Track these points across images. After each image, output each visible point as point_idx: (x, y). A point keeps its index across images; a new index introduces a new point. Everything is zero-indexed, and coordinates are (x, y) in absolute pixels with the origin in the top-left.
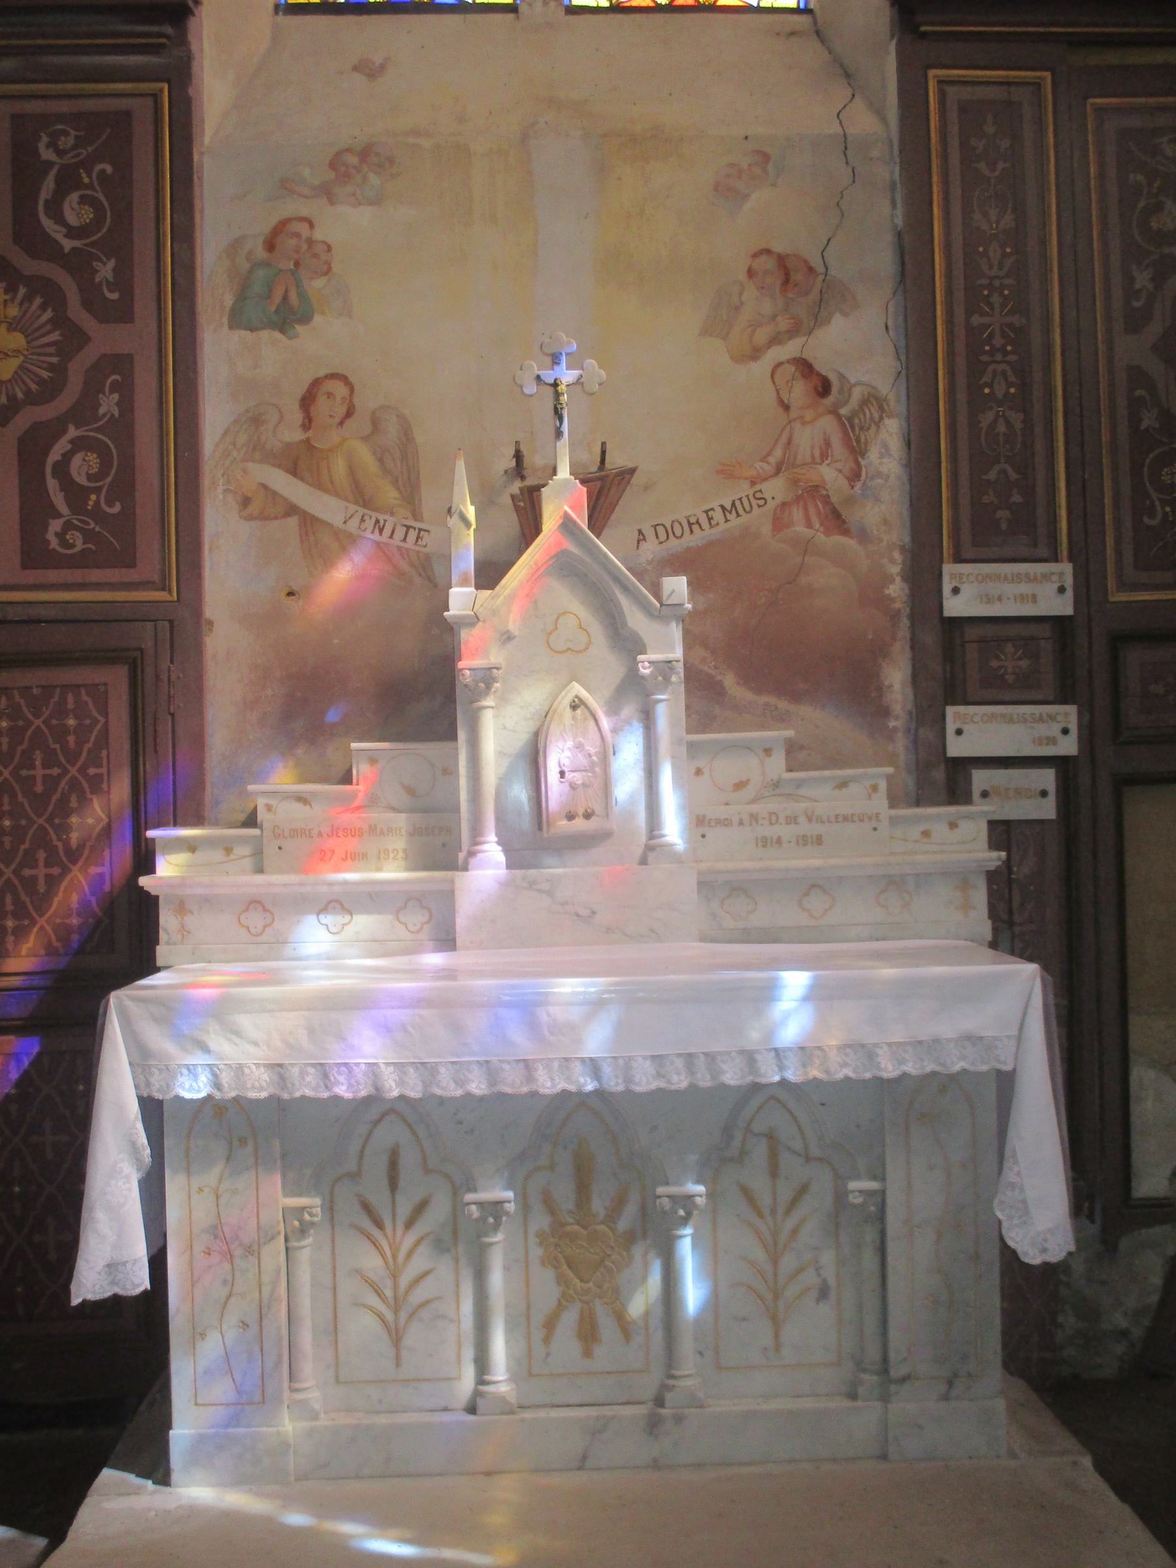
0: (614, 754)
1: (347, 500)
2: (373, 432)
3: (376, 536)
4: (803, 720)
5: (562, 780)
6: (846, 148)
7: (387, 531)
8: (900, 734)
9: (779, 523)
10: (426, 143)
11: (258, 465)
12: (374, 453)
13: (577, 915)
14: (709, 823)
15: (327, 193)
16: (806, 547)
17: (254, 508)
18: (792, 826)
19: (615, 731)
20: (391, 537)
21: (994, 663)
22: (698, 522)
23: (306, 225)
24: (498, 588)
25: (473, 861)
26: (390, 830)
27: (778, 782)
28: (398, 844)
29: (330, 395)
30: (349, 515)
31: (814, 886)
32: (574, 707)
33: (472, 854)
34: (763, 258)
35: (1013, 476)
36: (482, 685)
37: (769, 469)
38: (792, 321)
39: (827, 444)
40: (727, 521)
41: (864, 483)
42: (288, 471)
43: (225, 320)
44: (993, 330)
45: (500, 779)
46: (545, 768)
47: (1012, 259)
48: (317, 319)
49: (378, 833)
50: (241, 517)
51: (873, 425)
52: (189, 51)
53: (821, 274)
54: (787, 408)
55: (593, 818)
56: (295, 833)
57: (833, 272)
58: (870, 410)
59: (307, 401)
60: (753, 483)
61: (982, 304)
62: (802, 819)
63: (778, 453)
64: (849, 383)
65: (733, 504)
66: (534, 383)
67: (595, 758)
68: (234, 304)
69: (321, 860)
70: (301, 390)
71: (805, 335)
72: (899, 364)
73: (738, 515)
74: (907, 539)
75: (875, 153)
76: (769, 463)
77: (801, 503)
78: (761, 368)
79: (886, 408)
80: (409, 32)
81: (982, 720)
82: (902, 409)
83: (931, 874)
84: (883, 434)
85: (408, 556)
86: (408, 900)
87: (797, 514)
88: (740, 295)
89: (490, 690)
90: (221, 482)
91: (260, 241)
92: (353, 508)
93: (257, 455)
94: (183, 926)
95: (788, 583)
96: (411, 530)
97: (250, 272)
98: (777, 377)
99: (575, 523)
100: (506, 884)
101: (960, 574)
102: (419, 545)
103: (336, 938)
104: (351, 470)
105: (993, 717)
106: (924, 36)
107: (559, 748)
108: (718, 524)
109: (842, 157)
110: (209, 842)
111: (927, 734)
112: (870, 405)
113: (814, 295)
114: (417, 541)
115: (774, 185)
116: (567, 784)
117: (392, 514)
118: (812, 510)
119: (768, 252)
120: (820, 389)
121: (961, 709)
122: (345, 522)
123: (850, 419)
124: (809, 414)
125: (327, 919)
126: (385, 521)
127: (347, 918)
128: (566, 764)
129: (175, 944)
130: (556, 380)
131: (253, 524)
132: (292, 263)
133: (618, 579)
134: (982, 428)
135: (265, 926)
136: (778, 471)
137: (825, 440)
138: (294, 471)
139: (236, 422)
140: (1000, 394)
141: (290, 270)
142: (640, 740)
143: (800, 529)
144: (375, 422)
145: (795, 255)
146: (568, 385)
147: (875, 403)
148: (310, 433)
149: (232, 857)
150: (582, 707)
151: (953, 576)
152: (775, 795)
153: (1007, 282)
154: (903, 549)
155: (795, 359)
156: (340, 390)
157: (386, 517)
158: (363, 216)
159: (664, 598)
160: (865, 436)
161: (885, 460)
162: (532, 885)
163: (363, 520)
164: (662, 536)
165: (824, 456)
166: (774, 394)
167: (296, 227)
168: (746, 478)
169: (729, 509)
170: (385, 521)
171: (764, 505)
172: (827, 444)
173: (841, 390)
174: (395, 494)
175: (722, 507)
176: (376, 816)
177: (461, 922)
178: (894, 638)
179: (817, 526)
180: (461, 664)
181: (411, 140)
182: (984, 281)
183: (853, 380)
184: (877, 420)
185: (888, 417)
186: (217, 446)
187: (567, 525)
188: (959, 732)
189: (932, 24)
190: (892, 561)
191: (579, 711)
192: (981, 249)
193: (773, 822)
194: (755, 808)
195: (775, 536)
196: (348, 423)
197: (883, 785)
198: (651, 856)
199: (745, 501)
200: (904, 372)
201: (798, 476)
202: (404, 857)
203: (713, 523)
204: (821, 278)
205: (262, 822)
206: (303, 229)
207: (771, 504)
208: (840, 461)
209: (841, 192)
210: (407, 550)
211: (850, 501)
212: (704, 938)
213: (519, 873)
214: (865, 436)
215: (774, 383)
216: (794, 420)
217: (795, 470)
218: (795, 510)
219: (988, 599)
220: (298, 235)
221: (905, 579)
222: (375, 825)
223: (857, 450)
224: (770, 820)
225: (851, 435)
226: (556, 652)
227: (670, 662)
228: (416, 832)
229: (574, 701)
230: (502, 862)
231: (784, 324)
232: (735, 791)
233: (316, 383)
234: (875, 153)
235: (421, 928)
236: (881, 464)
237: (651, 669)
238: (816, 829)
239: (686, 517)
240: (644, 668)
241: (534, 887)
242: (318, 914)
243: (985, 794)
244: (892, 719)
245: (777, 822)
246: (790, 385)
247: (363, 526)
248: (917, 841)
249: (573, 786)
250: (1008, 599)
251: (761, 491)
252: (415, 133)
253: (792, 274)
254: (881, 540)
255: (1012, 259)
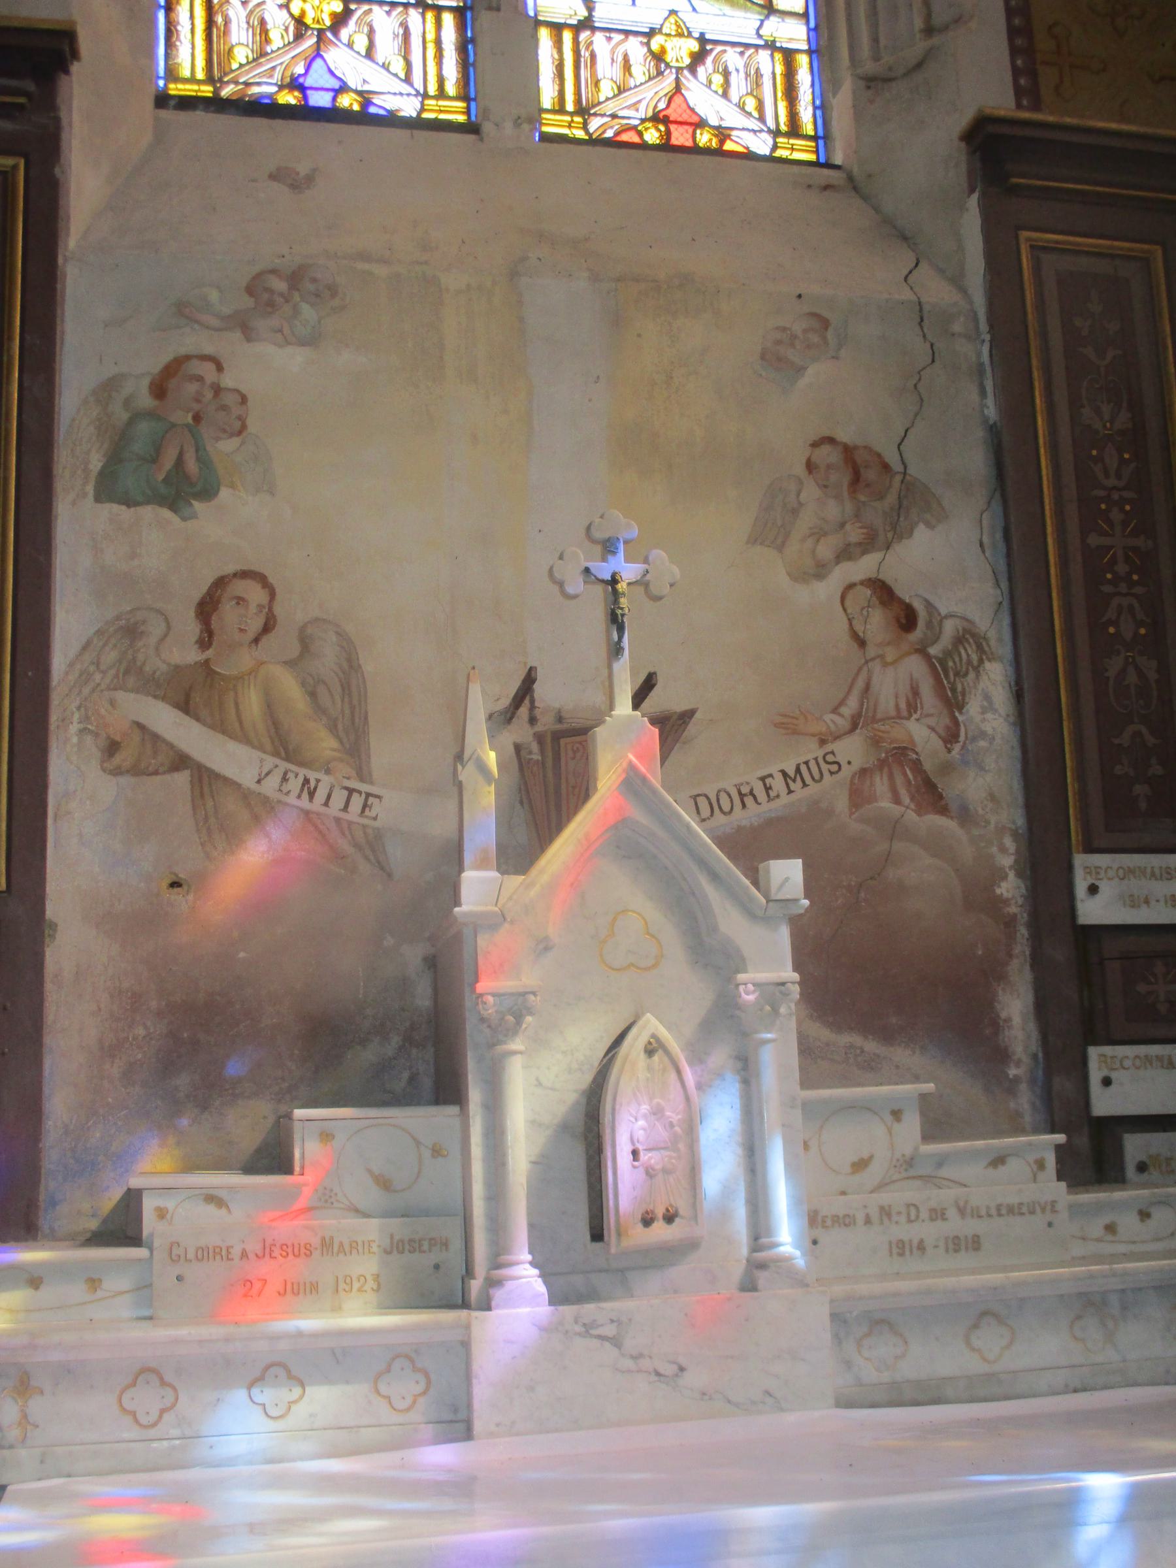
0: (701, 1123)
1: (261, 748)
2: (301, 656)
3: (304, 803)
4: (897, 1067)
5: (636, 1163)
6: (922, 320)
7: (321, 795)
8: (1023, 1087)
9: (858, 797)
10: (380, 271)
11: (132, 695)
12: (303, 684)
13: (658, 1374)
14: (824, 1221)
15: (243, 325)
16: (894, 830)
17: (123, 758)
18: (939, 1223)
19: (700, 1087)
20: (326, 804)
21: (1142, 988)
22: (751, 793)
23: (211, 366)
24: (534, 872)
25: (498, 1295)
26: (354, 1245)
27: (912, 1159)
28: (367, 1266)
29: (240, 600)
30: (265, 771)
31: (985, 1314)
32: (650, 1052)
33: (493, 1283)
34: (826, 449)
35: (1151, 741)
36: (510, 1018)
37: (843, 723)
38: (865, 531)
39: (915, 692)
40: (790, 792)
41: (963, 747)
42: (177, 706)
43: (90, 489)
44: (1114, 555)
45: (534, 1163)
46: (614, 1146)
47: (1133, 465)
48: (224, 493)
49: (336, 1249)
50: (104, 770)
51: (970, 669)
52: (57, 121)
53: (898, 473)
54: (862, 643)
55: (677, 1220)
56: (205, 1254)
57: (911, 471)
58: (966, 650)
59: (207, 608)
60: (823, 742)
61: (1100, 522)
62: (952, 1213)
63: (852, 704)
64: (939, 614)
65: (798, 770)
66: (581, 579)
67: (677, 1129)
68: (104, 467)
69: (245, 1295)
70: (198, 592)
71: (880, 550)
72: (999, 592)
73: (805, 785)
74: (1021, 821)
75: (957, 327)
76: (842, 716)
77: (886, 770)
78: (828, 589)
79: (986, 649)
80: (340, 142)
81: (1133, 1064)
82: (1006, 650)
83: (1140, 1289)
84: (984, 683)
85: (351, 833)
86: (393, 1359)
87: (880, 785)
88: (798, 495)
89: (521, 1027)
90: (76, 716)
91: (145, 382)
92: (270, 761)
93: (131, 681)
94: (25, 1416)
95: (871, 878)
96: (355, 796)
97: (131, 422)
98: (848, 603)
99: (644, 779)
100: (546, 1329)
101: (1096, 868)
102: (367, 817)
103: (272, 1425)
104: (269, 707)
105: (1148, 1059)
106: (1014, 191)
107: (631, 1115)
108: (778, 796)
109: (917, 329)
110: (61, 1271)
111: (1064, 1085)
112: (967, 646)
113: (891, 499)
114: (363, 811)
115: (836, 358)
116: (642, 1170)
117: (328, 772)
118: (899, 780)
119: (831, 440)
120: (903, 621)
121: (1108, 1050)
122: (259, 782)
123: (942, 662)
124: (891, 654)
125: (265, 1395)
126: (318, 781)
127: (297, 1391)
128: (641, 1139)
129: (11, 1447)
130: (614, 576)
131: (124, 780)
132: (190, 415)
133: (703, 864)
134: (1108, 678)
135: (163, 1411)
136: (854, 727)
137: (912, 688)
138: (185, 706)
139: (99, 633)
140: (1128, 635)
141: (187, 426)
142: (737, 1102)
143: (885, 803)
144: (305, 642)
145: (865, 447)
146: (629, 584)
147: (971, 640)
148: (210, 653)
149: (100, 1294)
150: (660, 1052)
151: (1087, 870)
152: (908, 1178)
153: (1127, 494)
154: (1015, 835)
155: (870, 579)
156: (255, 594)
157: (320, 775)
158: (293, 359)
159: (773, 890)
160: (963, 685)
161: (989, 716)
162: (588, 1329)
163: (285, 779)
164: (705, 811)
165: (912, 707)
166: (846, 626)
167: (197, 368)
168: (813, 735)
169: (793, 776)
170: (318, 781)
171: (837, 772)
172: (915, 692)
173: (929, 624)
174: (333, 743)
175: (784, 774)
176: (332, 1223)
177: (481, 1393)
178: (1010, 956)
179: (906, 800)
180: (481, 987)
181: (361, 266)
182: (1102, 493)
183: (943, 612)
184: (975, 663)
185: (989, 660)
186: (71, 665)
187: (633, 784)
188: (1107, 1082)
189: (1023, 176)
190: (1003, 850)
191: (656, 1058)
192: (1094, 452)
193: (913, 1217)
194: (885, 1198)
195: (854, 813)
196: (264, 640)
197: (1051, 1159)
198: (762, 1277)
199: (812, 764)
200: (1006, 604)
201: (880, 734)
202: (375, 1288)
203: (772, 794)
204: (898, 478)
205: (151, 1235)
206: (207, 371)
207: (846, 772)
208: (932, 715)
209: (919, 373)
210: (350, 823)
211: (947, 768)
212: (838, 1404)
213: (568, 1310)
214: (963, 685)
215: (845, 610)
216: (873, 659)
217: (876, 726)
218: (877, 779)
219: (1133, 902)
220: (200, 379)
221: (1020, 874)
222: (332, 1238)
223: (953, 703)
224: (909, 1214)
225: (945, 682)
226: (613, 969)
227: (783, 984)
228: (396, 1247)
229: (650, 1043)
230: (543, 1294)
231: (854, 534)
232: (853, 1173)
233: (220, 583)
234: (957, 327)
235: (414, 1402)
236: (984, 720)
237: (757, 994)
238: (971, 1227)
239: (736, 785)
240: (747, 993)
241: (594, 1332)
242: (250, 1387)
243: (1142, 1168)
244: (1012, 1065)
245: (918, 1217)
246: (865, 612)
247: (285, 788)
248: (1099, 1240)
249: (650, 1173)
250: (1158, 901)
251: (833, 753)
252: (364, 256)
253: (862, 470)
254: (988, 822)
255: (1133, 465)
